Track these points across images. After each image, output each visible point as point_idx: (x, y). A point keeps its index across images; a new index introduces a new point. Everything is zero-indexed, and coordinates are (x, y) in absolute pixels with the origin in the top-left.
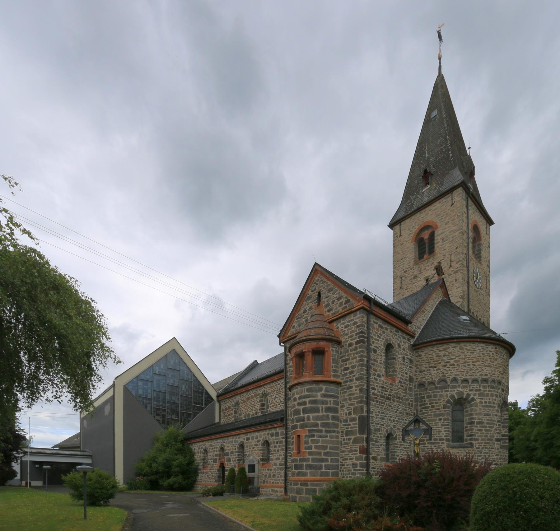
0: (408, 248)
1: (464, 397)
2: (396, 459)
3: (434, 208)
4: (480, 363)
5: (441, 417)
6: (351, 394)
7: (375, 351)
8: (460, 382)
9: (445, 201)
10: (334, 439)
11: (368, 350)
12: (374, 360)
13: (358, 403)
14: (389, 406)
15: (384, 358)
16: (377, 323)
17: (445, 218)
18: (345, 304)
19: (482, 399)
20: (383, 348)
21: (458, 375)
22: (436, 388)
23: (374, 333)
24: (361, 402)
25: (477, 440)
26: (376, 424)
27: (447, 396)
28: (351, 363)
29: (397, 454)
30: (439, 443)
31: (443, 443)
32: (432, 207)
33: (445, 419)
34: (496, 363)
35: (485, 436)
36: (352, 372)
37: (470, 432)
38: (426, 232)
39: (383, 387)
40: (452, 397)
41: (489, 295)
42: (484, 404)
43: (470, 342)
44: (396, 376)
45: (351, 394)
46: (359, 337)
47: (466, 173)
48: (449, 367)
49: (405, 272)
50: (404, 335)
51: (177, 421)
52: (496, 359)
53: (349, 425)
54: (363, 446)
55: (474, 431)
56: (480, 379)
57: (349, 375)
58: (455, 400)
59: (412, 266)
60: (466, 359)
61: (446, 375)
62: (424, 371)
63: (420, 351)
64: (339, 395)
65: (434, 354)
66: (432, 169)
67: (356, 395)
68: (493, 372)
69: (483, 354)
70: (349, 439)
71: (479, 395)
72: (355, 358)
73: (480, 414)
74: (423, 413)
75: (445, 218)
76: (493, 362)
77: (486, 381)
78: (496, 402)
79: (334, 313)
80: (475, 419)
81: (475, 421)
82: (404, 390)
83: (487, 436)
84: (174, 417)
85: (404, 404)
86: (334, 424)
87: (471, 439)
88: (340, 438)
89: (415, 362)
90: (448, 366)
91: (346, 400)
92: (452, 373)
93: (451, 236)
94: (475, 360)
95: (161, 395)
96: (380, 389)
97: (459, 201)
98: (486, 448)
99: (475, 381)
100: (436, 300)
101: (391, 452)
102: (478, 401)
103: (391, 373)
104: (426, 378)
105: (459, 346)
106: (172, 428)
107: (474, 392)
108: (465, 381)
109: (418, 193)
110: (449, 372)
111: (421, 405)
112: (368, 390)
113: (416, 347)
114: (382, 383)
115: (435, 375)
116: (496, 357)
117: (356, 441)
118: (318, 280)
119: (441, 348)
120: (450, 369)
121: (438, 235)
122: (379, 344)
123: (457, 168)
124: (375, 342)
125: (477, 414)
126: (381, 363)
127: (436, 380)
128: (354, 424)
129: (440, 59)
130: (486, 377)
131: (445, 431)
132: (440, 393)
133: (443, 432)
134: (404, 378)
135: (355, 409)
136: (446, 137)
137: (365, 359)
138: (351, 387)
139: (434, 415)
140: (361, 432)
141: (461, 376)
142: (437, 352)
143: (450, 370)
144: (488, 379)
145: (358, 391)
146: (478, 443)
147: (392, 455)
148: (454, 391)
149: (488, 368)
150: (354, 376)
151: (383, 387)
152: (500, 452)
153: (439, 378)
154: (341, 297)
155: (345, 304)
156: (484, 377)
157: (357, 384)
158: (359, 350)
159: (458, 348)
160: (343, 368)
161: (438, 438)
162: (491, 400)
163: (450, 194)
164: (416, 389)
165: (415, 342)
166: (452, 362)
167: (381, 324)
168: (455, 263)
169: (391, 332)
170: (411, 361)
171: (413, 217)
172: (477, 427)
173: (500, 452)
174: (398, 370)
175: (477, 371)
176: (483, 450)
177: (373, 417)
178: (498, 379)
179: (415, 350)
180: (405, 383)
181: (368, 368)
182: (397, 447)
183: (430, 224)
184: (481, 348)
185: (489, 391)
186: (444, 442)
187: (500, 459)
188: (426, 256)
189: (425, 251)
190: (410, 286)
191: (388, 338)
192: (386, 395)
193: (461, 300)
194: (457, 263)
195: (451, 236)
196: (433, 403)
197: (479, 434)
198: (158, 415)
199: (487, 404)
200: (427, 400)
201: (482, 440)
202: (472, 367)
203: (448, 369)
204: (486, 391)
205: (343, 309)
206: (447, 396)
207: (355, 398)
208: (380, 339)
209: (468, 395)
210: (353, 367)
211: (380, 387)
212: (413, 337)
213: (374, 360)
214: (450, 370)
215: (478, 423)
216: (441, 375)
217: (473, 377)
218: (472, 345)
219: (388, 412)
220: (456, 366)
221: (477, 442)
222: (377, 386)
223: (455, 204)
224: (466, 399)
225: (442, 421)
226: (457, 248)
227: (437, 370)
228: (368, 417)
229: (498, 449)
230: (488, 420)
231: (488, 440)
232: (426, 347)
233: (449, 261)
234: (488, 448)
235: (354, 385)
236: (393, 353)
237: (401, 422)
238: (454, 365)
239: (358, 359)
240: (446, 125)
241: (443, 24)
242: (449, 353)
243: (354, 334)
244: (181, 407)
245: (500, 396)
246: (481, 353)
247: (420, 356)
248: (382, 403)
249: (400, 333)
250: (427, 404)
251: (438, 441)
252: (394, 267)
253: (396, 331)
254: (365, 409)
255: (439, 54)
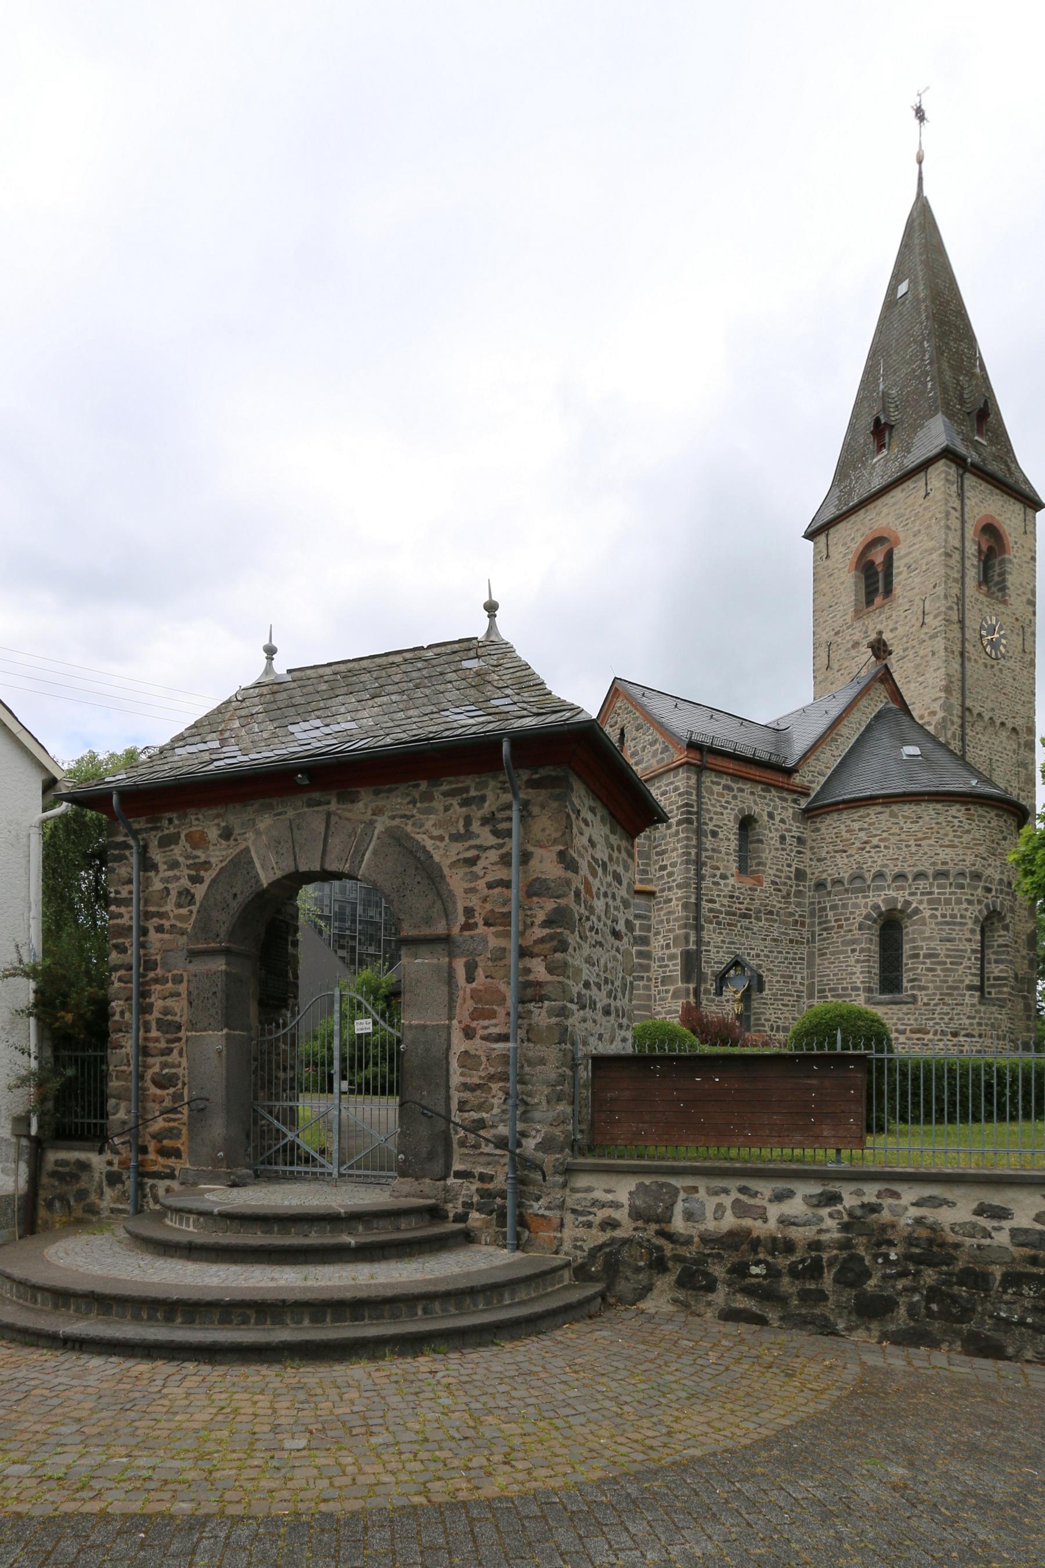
0: (842, 583)
1: (899, 906)
2: (763, 1025)
3: (893, 500)
4: (931, 842)
5: (854, 946)
6: (669, 913)
7: (714, 834)
8: (890, 879)
9: (912, 486)
10: (641, 992)
11: (699, 833)
12: (713, 850)
13: (680, 928)
14: (747, 929)
15: (734, 844)
16: (718, 784)
17: (913, 522)
18: (661, 753)
19: (936, 909)
20: (734, 826)
21: (886, 866)
22: (847, 891)
23: (713, 802)
24: (685, 926)
25: (925, 988)
26: (715, 963)
27: (866, 905)
28: (670, 858)
29: (768, 1016)
30: (850, 995)
31: (859, 995)
32: (888, 499)
33: (862, 950)
34: (966, 838)
35: (941, 981)
36: (671, 874)
37: (911, 974)
38: (879, 548)
39: (732, 897)
40: (876, 907)
41: (1032, 664)
42: (940, 919)
43: (910, 802)
44: (764, 872)
45: (669, 913)
46: (682, 813)
47: (969, 413)
48: (869, 852)
49: (837, 634)
50: (785, 795)
51: (377, 957)
52: (968, 832)
53: (667, 966)
54: (688, 1003)
55: (919, 971)
56: (930, 872)
57: (666, 879)
58: (880, 914)
59: (849, 620)
60: (903, 836)
61: (865, 866)
62: (825, 859)
63: (819, 820)
64: (652, 914)
65: (843, 827)
66: (895, 416)
67: (677, 915)
68: (961, 857)
69: (937, 823)
70: (667, 991)
71: (930, 902)
72: (675, 849)
73: (930, 938)
74: (824, 939)
75: (913, 522)
76: (961, 837)
77: (944, 874)
78: (968, 914)
79: (646, 769)
80: (922, 948)
81: (921, 953)
82: (783, 897)
83: (947, 981)
84: (371, 950)
85: (786, 923)
86: (640, 965)
87: (913, 988)
88: (653, 989)
89: (809, 843)
90: (868, 849)
91: (662, 921)
92: (874, 862)
93: (924, 561)
94: (920, 835)
95: (348, 911)
96: (725, 901)
97: (939, 488)
98: (944, 1004)
99: (920, 875)
100: (867, 711)
101: (755, 1014)
102: (927, 913)
103: (754, 868)
104: (830, 873)
105: (888, 810)
106: (367, 973)
107: (919, 897)
108: (900, 876)
109: (863, 464)
110: (870, 860)
111: (820, 924)
112: (698, 905)
113: (811, 814)
114: (730, 888)
115: (842, 867)
116: (967, 827)
117: (676, 995)
118: (620, 708)
119: (855, 816)
120: (872, 854)
121: (900, 558)
122: (724, 820)
123: (940, 414)
124: (715, 817)
125: (924, 939)
126: (727, 854)
127: (847, 875)
128: (674, 965)
129: (920, 162)
130: (945, 868)
131: (862, 972)
132: (854, 900)
133: (858, 975)
134: (783, 875)
135: (676, 938)
136: (922, 343)
137: (693, 851)
138: (670, 900)
139: (842, 942)
140: (687, 977)
141: (891, 866)
142: (849, 822)
143: (871, 857)
144: (948, 871)
145: (680, 908)
146: (927, 995)
147: (756, 1020)
148: (880, 895)
149: (948, 850)
150: (674, 881)
151: (732, 897)
152: (978, 1012)
153: (851, 872)
154: (656, 741)
155: (661, 753)
156: (939, 867)
157: (680, 895)
158: (682, 835)
159: (887, 814)
160: (657, 867)
161: (849, 986)
162: (956, 912)
163: (923, 474)
164: (811, 893)
165: (810, 803)
166: (875, 841)
167: (729, 783)
168: (931, 616)
169: (752, 793)
170: (800, 841)
171: (853, 518)
172: (924, 963)
173: (978, 1012)
174: (769, 862)
175: (925, 857)
176: (938, 1008)
177: (709, 951)
178: (973, 869)
179: (809, 818)
180: (785, 884)
181: (699, 864)
182: (766, 1004)
183: (885, 535)
184: (932, 813)
185: (950, 894)
186: (861, 993)
187: (980, 1024)
188: (878, 600)
189: (877, 589)
190: (847, 664)
191: (745, 806)
192: (740, 909)
193: (943, 694)
194: (935, 617)
195: (924, 561)
196: (840, 920)
197: (930, 977)
198: (342, 947)
199: (948, 919)
200: (831, 914)
201: (936, 988)
202: (913, 849)
203: (867, 855)
204: (945, 893)
205: (658, 762)
206: (866, 905)
207: (675, 920)
208: (725, 812)
209: (908, 903)
210: (673, 865)
211: (724, 897)
212: (807, 795)
213: (713, 850)
214: (871, 857)
215: (926, 956)
216: (855, 867)
217: (915, 870)
218: (914, 807)
219: (743, 940)
220: (882, 849)
221: (924, 992)
222: (719, 896)
223: (931, 495)
224: (902, 911)
225: (857, 953)
226: (934, 587)
227: (847, 857)
228: (698, 952)
229: (973, 1005)
230: (948, 950)
231: (948, 988)
232: (827, 813)
233: (920, 612)
234: (949, 1005)
235: (674, 897)
236: (758, 830)
237: (776, 958)
238: (877, 846)
239: (680, 851)
240: (923, 317)
241: (928, 88)
242: (870, 824)
243: (674, 807)
244: (385, 929)
245: (979, 902)
246: (934, 821)
247: (818, 830)
248: (729, 924)
249: (774, 792)
250: (830, 921)
251: (850, 992)
252: (816, 624)
253: (762, 790)
254: (692, 938)
255: (918, 153)
